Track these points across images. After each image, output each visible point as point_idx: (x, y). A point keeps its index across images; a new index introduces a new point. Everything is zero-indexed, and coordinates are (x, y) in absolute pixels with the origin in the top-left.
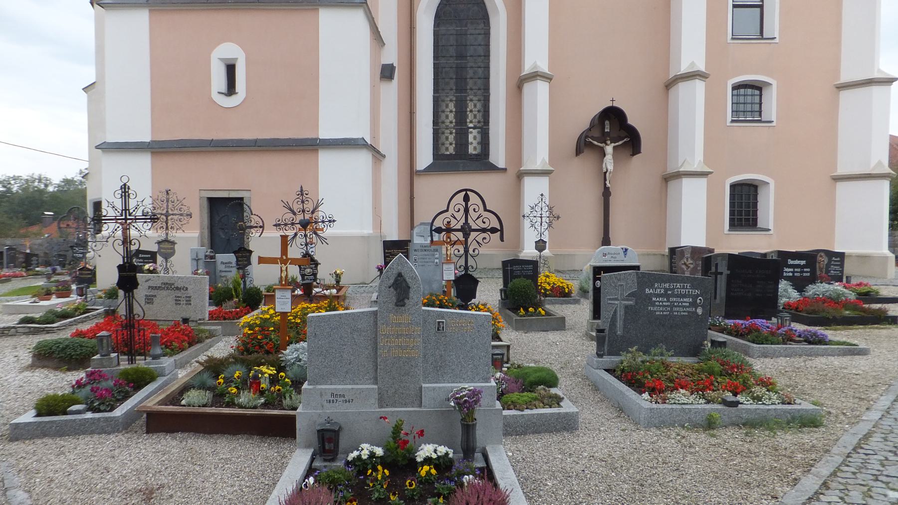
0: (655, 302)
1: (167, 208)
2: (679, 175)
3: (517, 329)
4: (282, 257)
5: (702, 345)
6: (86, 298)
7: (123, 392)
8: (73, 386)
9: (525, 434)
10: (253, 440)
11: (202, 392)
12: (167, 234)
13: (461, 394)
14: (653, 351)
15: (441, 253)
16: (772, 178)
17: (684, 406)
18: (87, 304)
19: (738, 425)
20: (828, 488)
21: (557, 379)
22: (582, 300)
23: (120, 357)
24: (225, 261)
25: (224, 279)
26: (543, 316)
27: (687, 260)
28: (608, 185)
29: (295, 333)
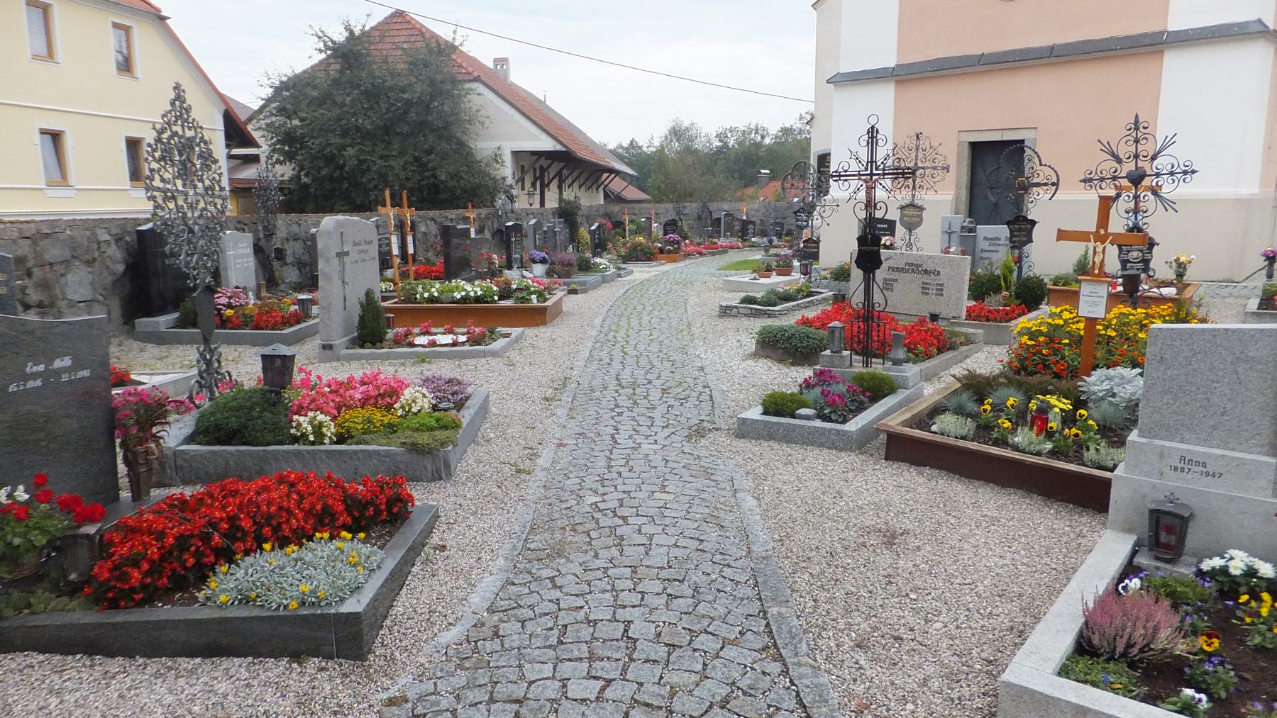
1: (916, 159)
4: (1097, 231)
6: (810, 277)
7: (857, 402)
8: (800, 386)
10: (1032, 500)
11: (962, 420)
12: (913, 196)
18: (811, 285)
23: (854, 357)
24: (989, 237)
25: (986, 262)
29: (1104, 351)
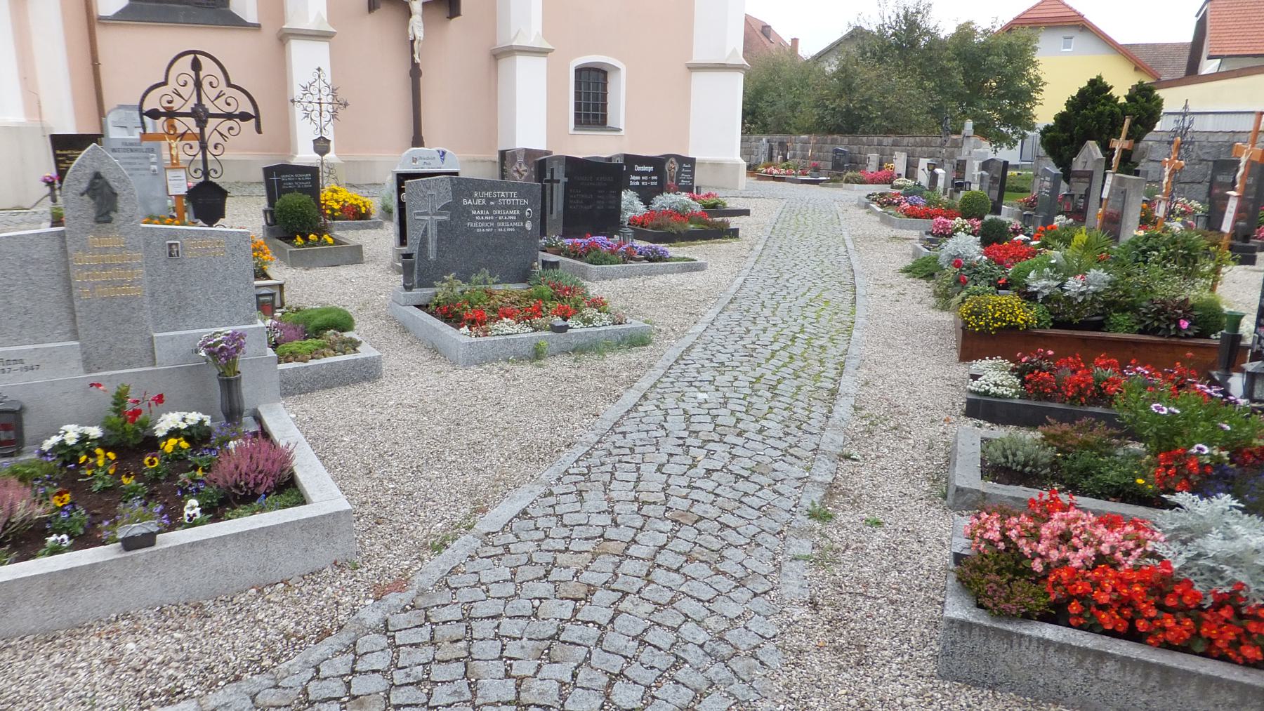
0: (475, 215)
2: (511, 51)
3: (293, 265)
5: (532, 267)
9: (312, 390)
13: (215, 340)
14: (474, 278)
15: (160, 156)
16: (622, 61)
17: (508, 337)
19: (567, 352)
20: (646, 399)
21: (351, 320)
22: (386, 223)
26: (331, 245)
27: (520, 166)
28: (417, 60)
